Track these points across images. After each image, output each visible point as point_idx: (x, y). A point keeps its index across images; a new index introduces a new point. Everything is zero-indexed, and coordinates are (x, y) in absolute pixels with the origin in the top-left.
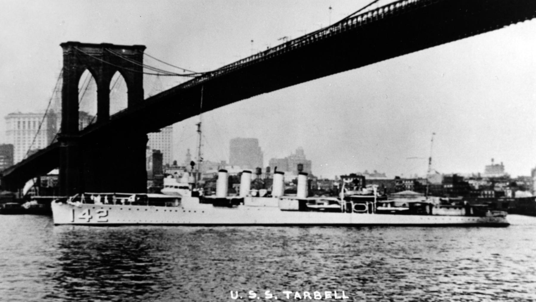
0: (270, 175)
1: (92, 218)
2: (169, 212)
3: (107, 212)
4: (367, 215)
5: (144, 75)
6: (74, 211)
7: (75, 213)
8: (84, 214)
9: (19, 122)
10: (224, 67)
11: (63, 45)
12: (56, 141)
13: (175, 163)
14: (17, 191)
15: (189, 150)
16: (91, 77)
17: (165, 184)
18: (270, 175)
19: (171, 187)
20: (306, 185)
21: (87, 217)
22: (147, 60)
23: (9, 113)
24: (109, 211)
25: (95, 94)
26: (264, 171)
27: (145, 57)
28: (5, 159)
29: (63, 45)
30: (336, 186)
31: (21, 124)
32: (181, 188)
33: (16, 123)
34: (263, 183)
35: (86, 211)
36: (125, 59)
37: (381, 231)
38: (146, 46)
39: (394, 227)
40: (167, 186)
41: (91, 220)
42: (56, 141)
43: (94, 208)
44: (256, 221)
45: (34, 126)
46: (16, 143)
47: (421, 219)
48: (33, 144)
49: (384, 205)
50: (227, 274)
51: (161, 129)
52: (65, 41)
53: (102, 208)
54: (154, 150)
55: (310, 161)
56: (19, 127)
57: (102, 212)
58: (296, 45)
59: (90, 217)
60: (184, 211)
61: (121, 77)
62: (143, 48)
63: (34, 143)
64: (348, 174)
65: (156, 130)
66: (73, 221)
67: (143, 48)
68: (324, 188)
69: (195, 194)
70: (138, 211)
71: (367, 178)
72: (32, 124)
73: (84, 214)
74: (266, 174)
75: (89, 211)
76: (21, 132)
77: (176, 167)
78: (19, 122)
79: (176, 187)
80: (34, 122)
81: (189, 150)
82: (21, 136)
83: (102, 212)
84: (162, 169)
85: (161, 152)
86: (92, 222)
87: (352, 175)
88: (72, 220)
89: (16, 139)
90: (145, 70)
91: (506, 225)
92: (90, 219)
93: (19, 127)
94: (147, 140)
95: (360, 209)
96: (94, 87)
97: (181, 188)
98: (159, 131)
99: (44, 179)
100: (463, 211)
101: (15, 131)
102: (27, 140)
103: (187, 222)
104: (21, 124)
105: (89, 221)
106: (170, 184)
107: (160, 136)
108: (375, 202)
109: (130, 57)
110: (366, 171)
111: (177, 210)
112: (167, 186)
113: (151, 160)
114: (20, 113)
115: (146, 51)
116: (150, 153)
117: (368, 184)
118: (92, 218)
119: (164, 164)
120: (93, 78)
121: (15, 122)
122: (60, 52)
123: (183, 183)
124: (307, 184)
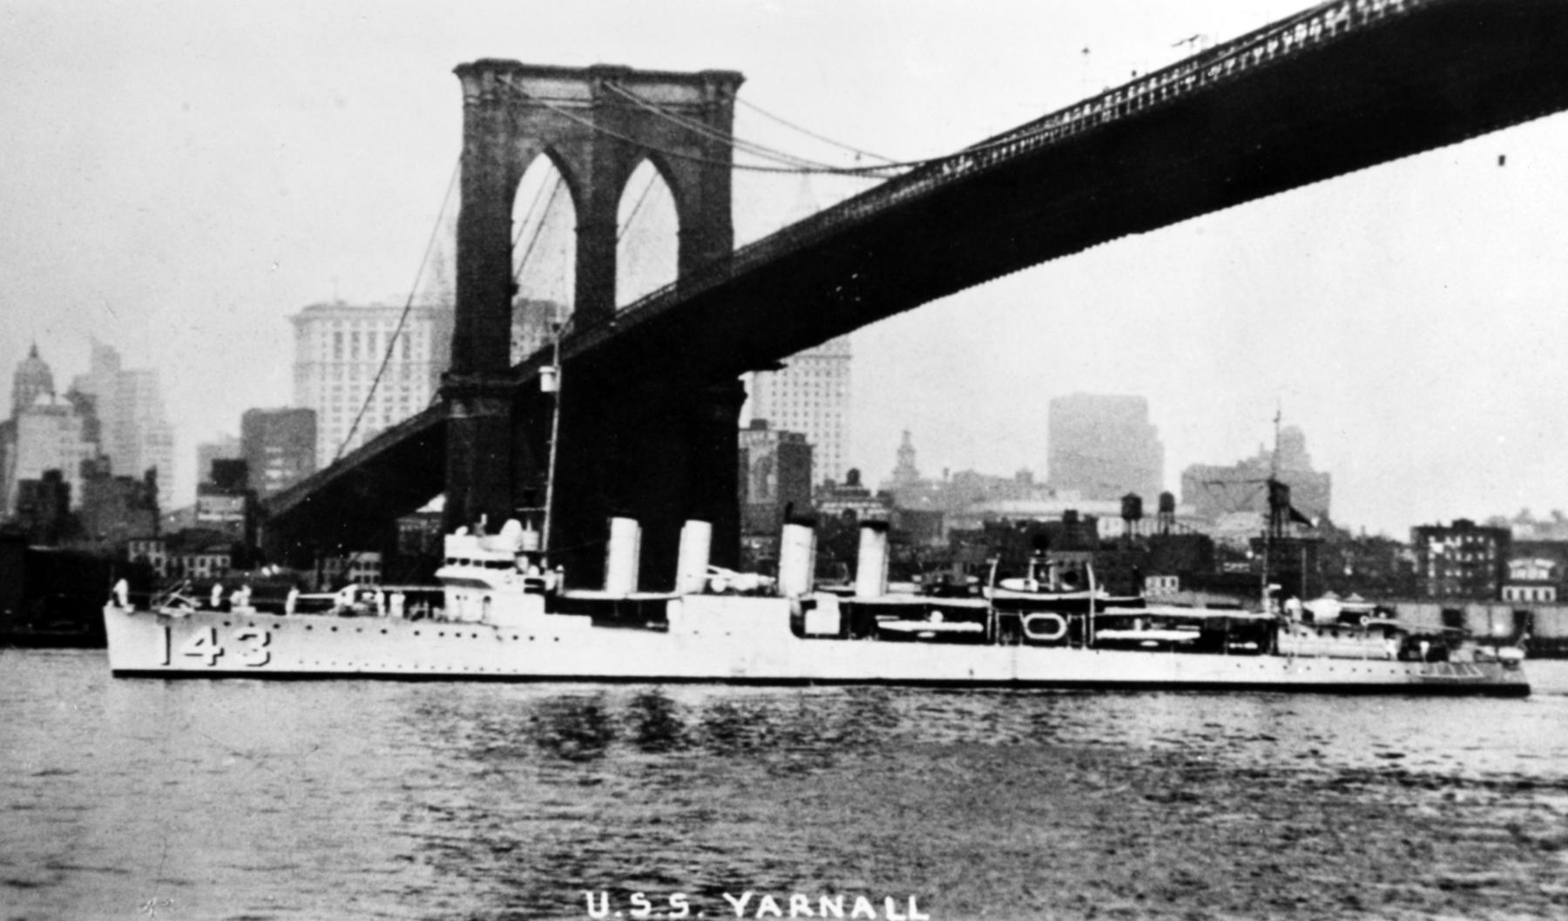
0: (1173, 521)
1: (222, 653)
2: (528, 640)
3: (268, 636)
4: (1066, 653)
5: (736, 175)
6: (168, 632)
7: (174, 633)
8: (200, 643)
9: (338, 337)
10: (972, 147)
11: (463, 71)
12: (439, 400)
13: (854, 476)
14: (309, 567)
15: (907, 434)
16: (558, 186)
17: (449, 553)
18: (1173, 521)
19: (465, 562)
20: (884, 563)
21: (209, 650)
22: (747, 122)
23: (310, 302)
24: (274, 633)
25: (570, 240)
26: (1151, 507)
27: (740, 109)
28: (285, 455)
29: (463, 71)
30: (1409, 564)
31: (347, 339)
32: (491, 565)
33: (330, 340)
34: (1148, 550)
35: (205, 632)
36: (670, 118)
37: (1118, 702)
38: (746, 74)
39: (1286, 697)
40: (452, 561)
41: (219, 659)
42: (439, 400)
43: (227, 624)
44: (971, 672)
45: (372, 347)
46: (328, 405)
47: (1178, 665)
48: (366, 408)
49: (1138, 623)
50: (1224, 872)
51: (783, 361)
52: (471, 58)
53: (251, 625)
54: (781, 434)
55: (1326, 476)
56: (338, 350)
57: (254, 636)
58: (1189, 81)
59: (216, 650)
60: (499, 638)
61: (660, 180)
62: (736, 80)
63: (371, 404)
64: (1447, 523)
65: (770, 362)
66: (168, 663)
67: (736, 80)
68: (1363, 570)
69: (535, 587)
70: (333, 633)
71: (1518, 532)
72: (364, 342)
73: (200, 643)
74: (1160, 519)
75: (214, 632)
76: (346, 369)
77: (856, 493)
78: (338, 337)
79: (478, 563)
80: (372, 337)
81: (907, 434)
82: (346, 382)
83: (254, 636)
84: (808, 497)
85: (810, 440)
86: (223, 665)
87: (1462, 527)
88: (164, 660)
89: (329, 393)
90: (738, 157)
91: (1520, 691)
92: (215, 656)
93: (338, 350)
94: (739, 396)
95: (1075, 638)
96: (567, 216)
97: (491, 565)
98: (775, 367)
99: (410, 528)
100: (1392, 646)
101: (323, 365)
102: (346, 393)
103: (391, 668)
104: (347, 339)
105: (214, 663)
106: (460, 555)
107: (774, 384)
108: (1092, 614)
109: (688, 109)
110: (1525, 512)
111: (359, 626)
112: (452, 561)
113: (775, 468)
114: (341, 305)
115: (743, 93)
116: (771, 442)
117: (1517, 557)
118: (222, 653)
119: (818, 479)
120: (564, 185)
121: (324, 335)
122: (453, 95)
123: (498, 551)
124: (887, 560)
